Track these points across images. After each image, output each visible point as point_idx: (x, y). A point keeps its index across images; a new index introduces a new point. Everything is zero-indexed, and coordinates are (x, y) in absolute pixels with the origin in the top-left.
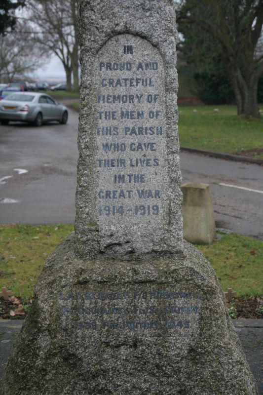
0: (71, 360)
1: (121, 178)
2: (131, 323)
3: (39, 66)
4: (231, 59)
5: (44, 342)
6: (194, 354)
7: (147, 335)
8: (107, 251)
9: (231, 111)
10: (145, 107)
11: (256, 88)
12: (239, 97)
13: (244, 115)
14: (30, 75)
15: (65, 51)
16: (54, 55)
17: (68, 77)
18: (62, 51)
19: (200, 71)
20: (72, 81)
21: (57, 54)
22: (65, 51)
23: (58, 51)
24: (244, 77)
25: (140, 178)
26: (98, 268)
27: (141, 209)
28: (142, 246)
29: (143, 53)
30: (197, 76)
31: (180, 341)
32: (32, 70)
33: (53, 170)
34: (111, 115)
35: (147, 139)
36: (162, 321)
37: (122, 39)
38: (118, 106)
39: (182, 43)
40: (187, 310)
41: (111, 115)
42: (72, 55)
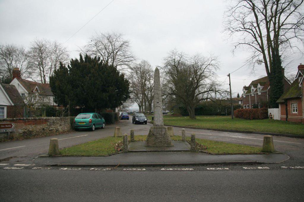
0: (154, 134)
1: (157, 119)
2: (159, 131)
3: (130, 106)
4: (187, 103)
5: (151, 133)
6: (164, 134)
7: (160, 132)
8: (156, 126)
9: (188, 118)
10: (159, 113)
11: (194, 111)
12: (189, 113)
13: (191, 118)
14: (128, 109)
15: (139, 101)
16: (135, 102)
17: (140, 109)
18: (138, 101)
19: (181, 106)
20: (141, 110)
21: (137, 102)
22: (139, 101)
23: (137, 101)
24: (191, 108)
25: (159, 119)
26: (156, 127)
27: (159, 122)
28: (160, 125)
29: (159, 108)
30: (180, 108)
31: (163, 133)
32: (128, 107)
33: (142, 130)
34: (156, 113)
35: (160, 115)
36: (162, 131)
37: (158, 107)
38: (157, 113)
39: (175, 98)
40: (164, 130)
41: (156, 113)
42: (142, 102)
